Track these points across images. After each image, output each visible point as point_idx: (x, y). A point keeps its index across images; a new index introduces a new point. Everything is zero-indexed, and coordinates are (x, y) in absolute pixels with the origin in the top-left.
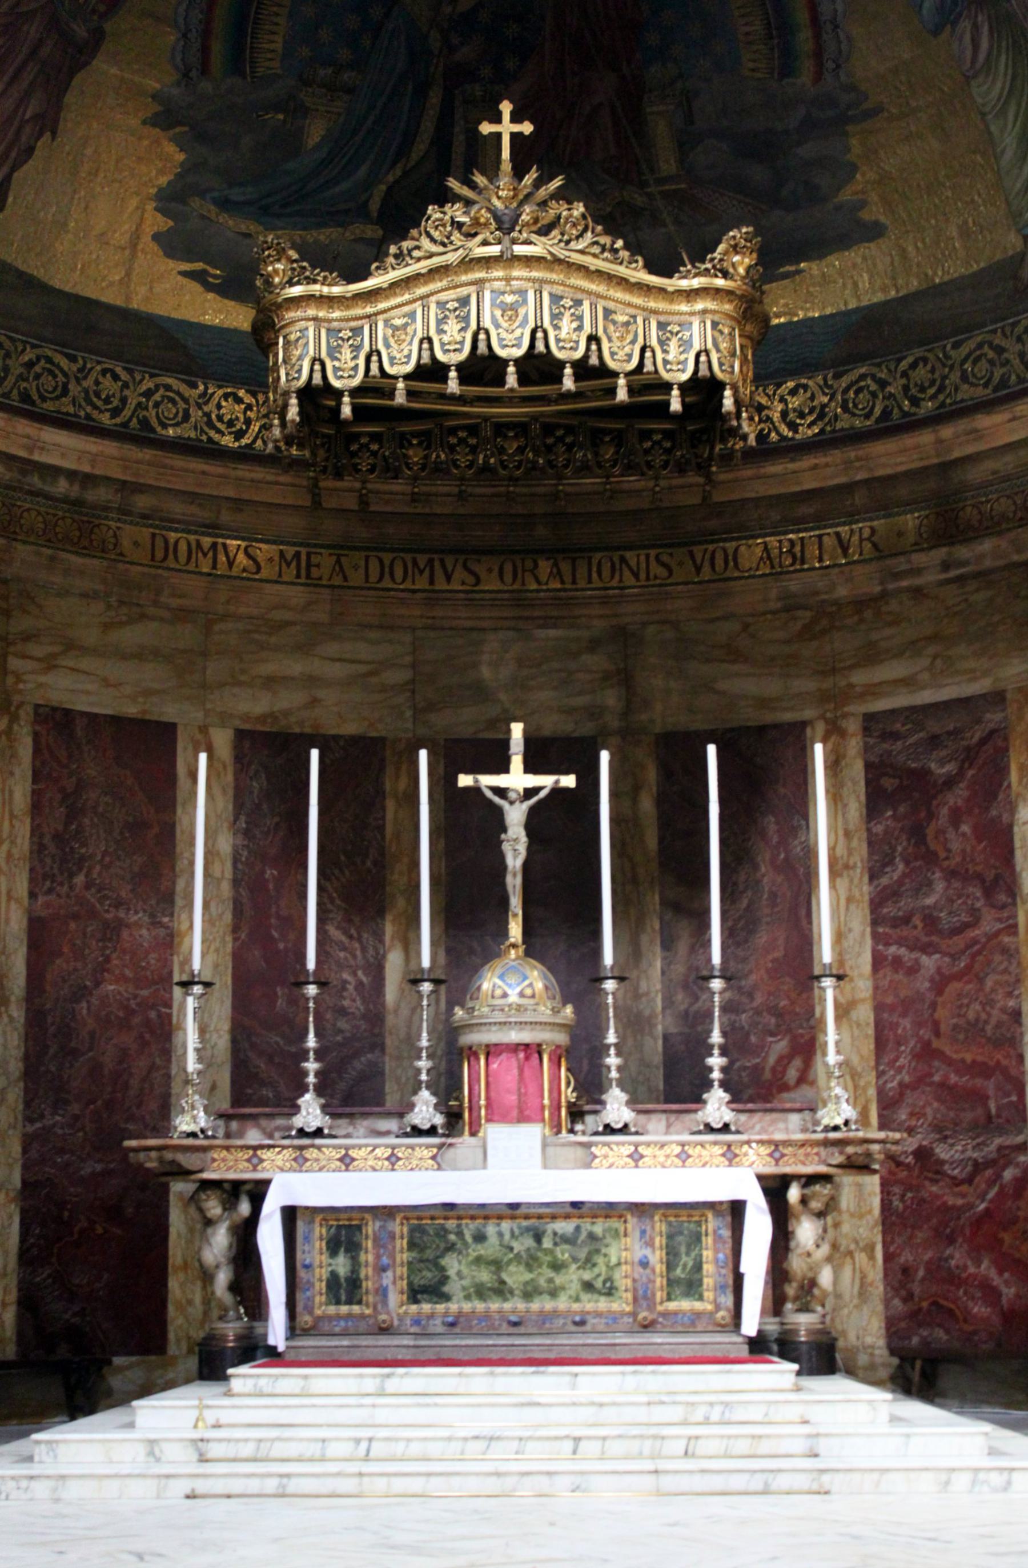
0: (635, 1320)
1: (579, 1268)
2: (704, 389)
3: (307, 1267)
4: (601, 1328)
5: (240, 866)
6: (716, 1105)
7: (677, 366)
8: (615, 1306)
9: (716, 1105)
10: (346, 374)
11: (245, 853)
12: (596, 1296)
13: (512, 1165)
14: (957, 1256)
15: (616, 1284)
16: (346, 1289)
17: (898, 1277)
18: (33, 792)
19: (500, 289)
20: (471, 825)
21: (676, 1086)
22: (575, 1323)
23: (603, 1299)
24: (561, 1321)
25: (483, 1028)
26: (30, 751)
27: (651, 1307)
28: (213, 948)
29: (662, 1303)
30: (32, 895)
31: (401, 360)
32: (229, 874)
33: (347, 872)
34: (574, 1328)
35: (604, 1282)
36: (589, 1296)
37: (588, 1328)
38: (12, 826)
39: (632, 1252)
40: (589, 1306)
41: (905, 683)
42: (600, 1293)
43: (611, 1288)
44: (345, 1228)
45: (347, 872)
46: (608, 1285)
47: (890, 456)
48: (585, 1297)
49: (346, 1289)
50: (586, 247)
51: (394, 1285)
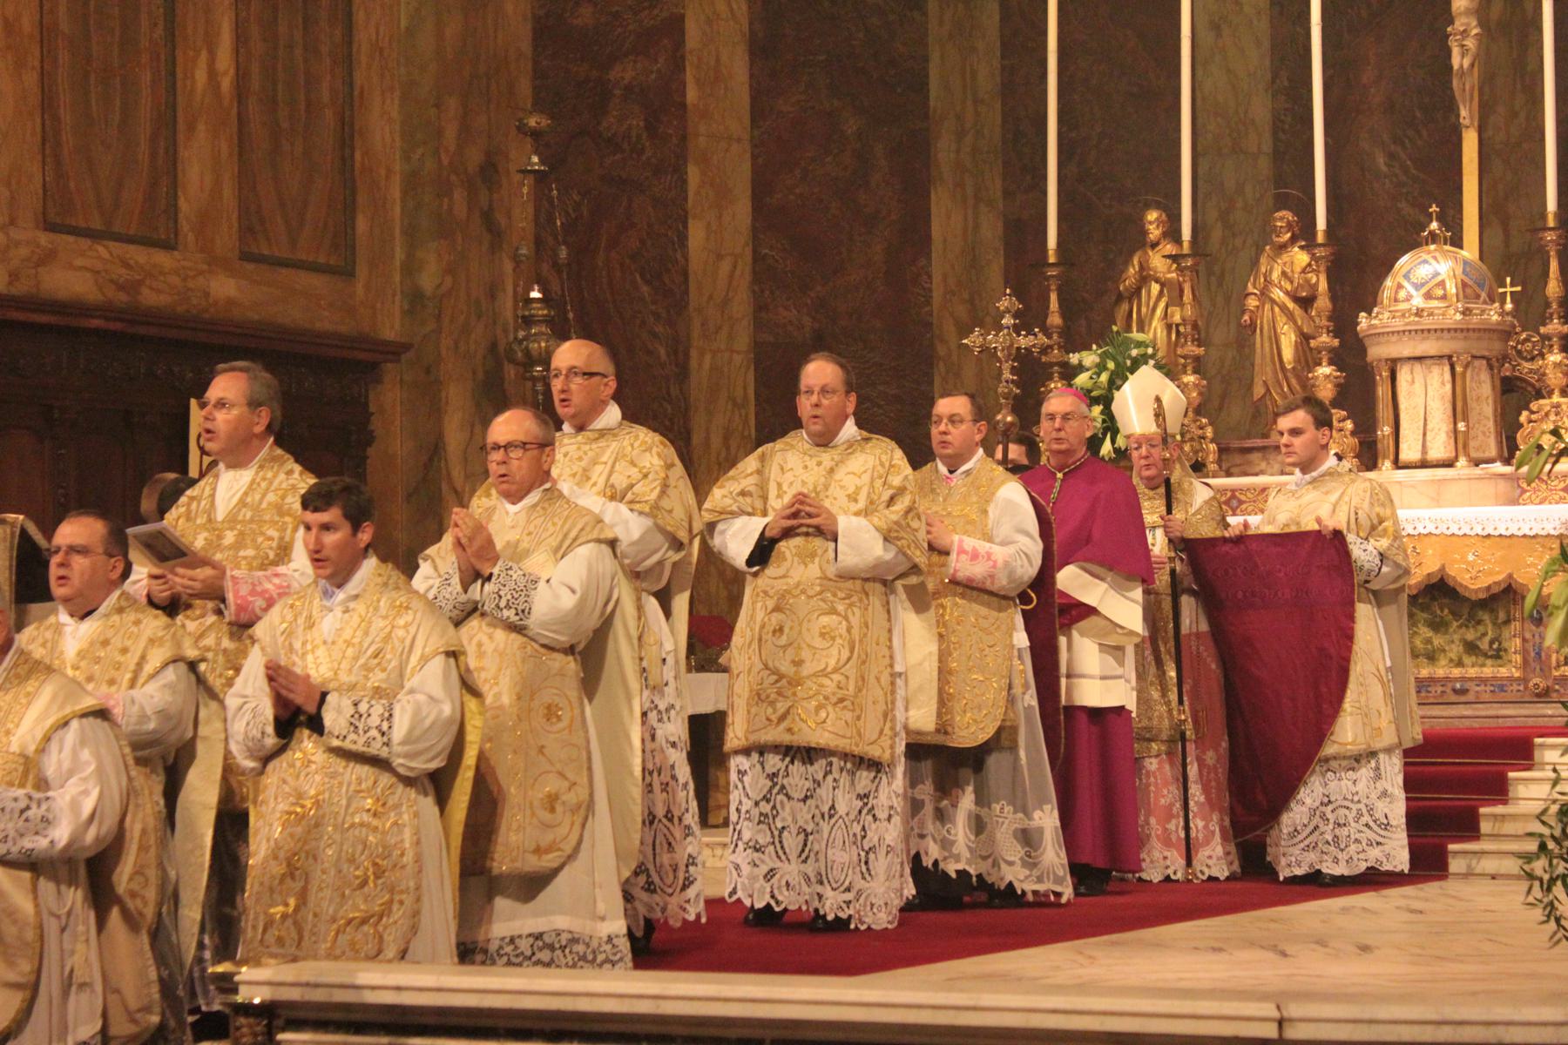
0: (1526, 688)
1: (1460, 627)
3: (137, 623)
4: (1487, 697)
5: (1281, 135)
8: (1503, 672)
11: (1289, 119)
12: (1481, 659)
15: (1505, 645)
18: (1003, 68)
22: (1455, 691)
23: (1489, 662)
24: (1440, 689)
25: (1382, 339)
26: (997, 17)
27: (1545, 671)
28: (1250, 241)
29: (1558, 666)
30: (1007, 194)
32: (1267, 146)
33: (1425, 133)
34: (1454, 698)
35: (1491, 643)
36: (1474, 658)
37: (1471, 697)
38: (977, 114)
40: (1472, 672)
42: (1486, 656)
43: (1499, 650)
45: (1425, 133)
46: (1495, 646)
48: (1467, 660)
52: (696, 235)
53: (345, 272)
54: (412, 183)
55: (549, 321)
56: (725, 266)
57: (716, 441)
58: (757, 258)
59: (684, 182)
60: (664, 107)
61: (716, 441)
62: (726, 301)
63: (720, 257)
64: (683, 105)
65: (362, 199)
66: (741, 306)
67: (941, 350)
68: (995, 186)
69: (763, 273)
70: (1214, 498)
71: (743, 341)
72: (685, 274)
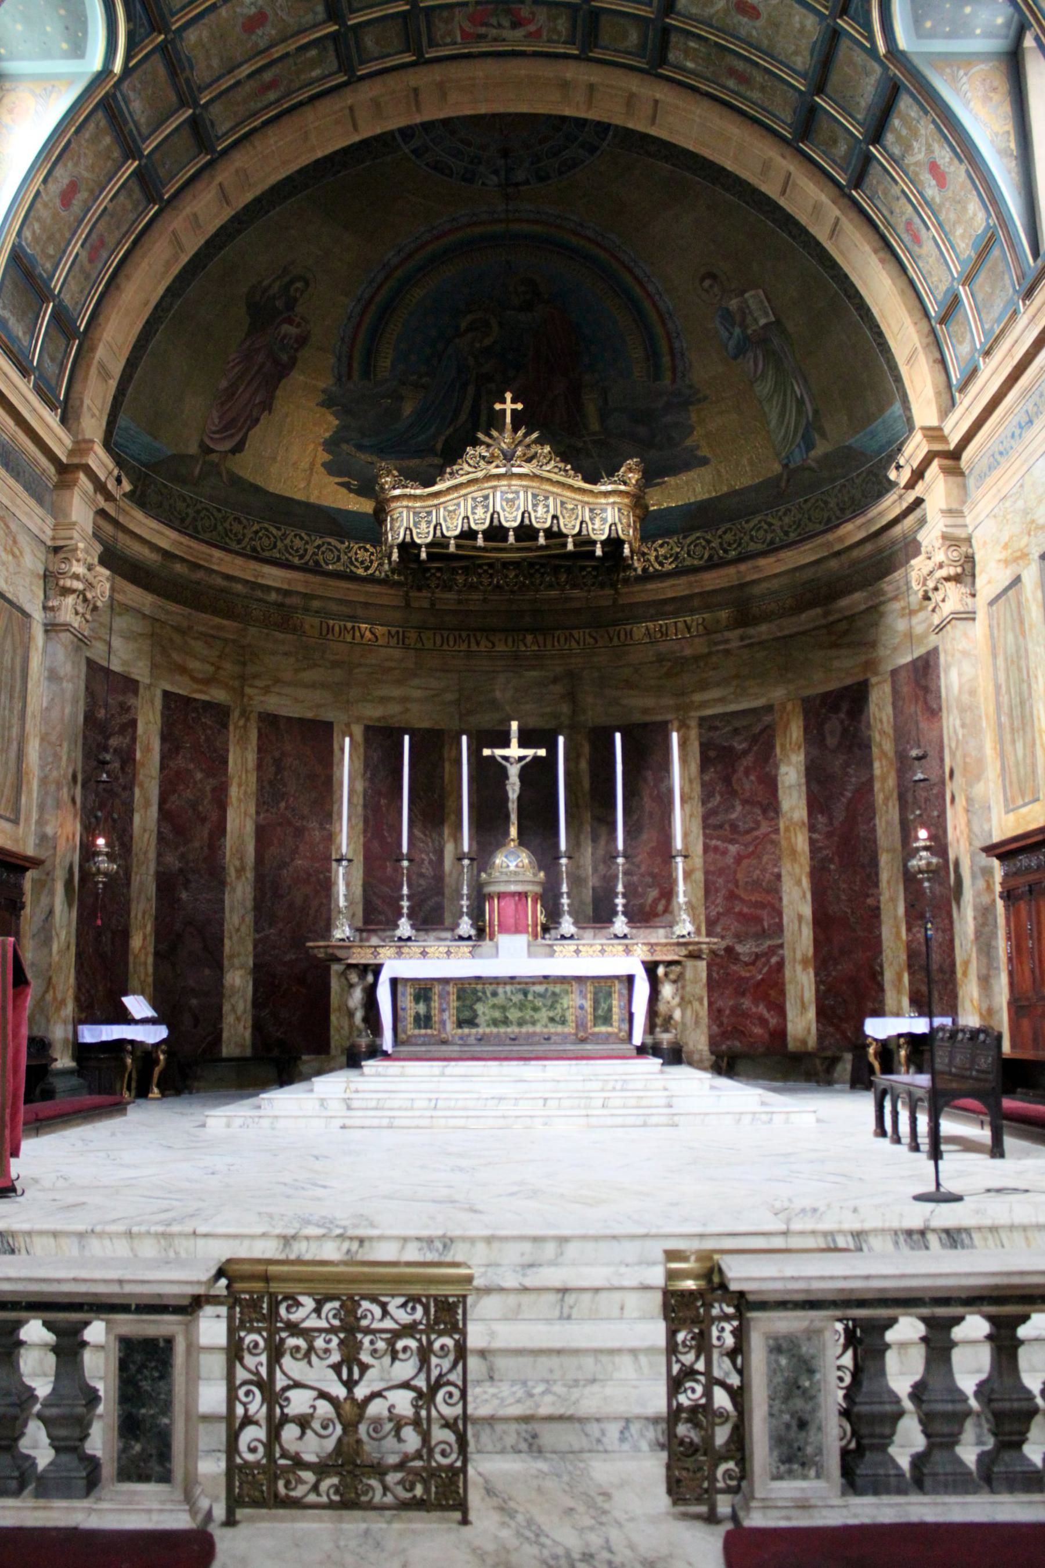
2: (614, 544)
6: (620, 924)
7: (599, 531)
9: (620, 924)
10: (423, 536)
13: (512, 956)
14: (746, 1003)
16: (424, 1021)
17: (715, 1013)
19: (504, 492)
20: (490, 775)
21: (598, 915)
30: (258, 813)
31: (453, 528)
32: (361, 801)
39: (576, 1003)
40: (553, 1030)
41: (717, 701)
44: (423, 989)
47: (713, 580)
49: (424, 1021)
50: (551, 469)
51: (449, 1018)
52: (137, 818)
53: (16, 822)
54: (44, 781)
55: (107, 854)
56: (146, 836)
57: (140, 916)
58: (159, 833)
59: (133, 794)
60: (127, 758)
61: (140, 916)
62: (146, 853)
63: (145, 831)
64: (134, 760)
65: (24, 788)
66: (152, 855)
67: (228, 880)
68: (252, 810)
69: (161, 838)
70: (922, 996)
71: (152, 871)
72: (131, 837)
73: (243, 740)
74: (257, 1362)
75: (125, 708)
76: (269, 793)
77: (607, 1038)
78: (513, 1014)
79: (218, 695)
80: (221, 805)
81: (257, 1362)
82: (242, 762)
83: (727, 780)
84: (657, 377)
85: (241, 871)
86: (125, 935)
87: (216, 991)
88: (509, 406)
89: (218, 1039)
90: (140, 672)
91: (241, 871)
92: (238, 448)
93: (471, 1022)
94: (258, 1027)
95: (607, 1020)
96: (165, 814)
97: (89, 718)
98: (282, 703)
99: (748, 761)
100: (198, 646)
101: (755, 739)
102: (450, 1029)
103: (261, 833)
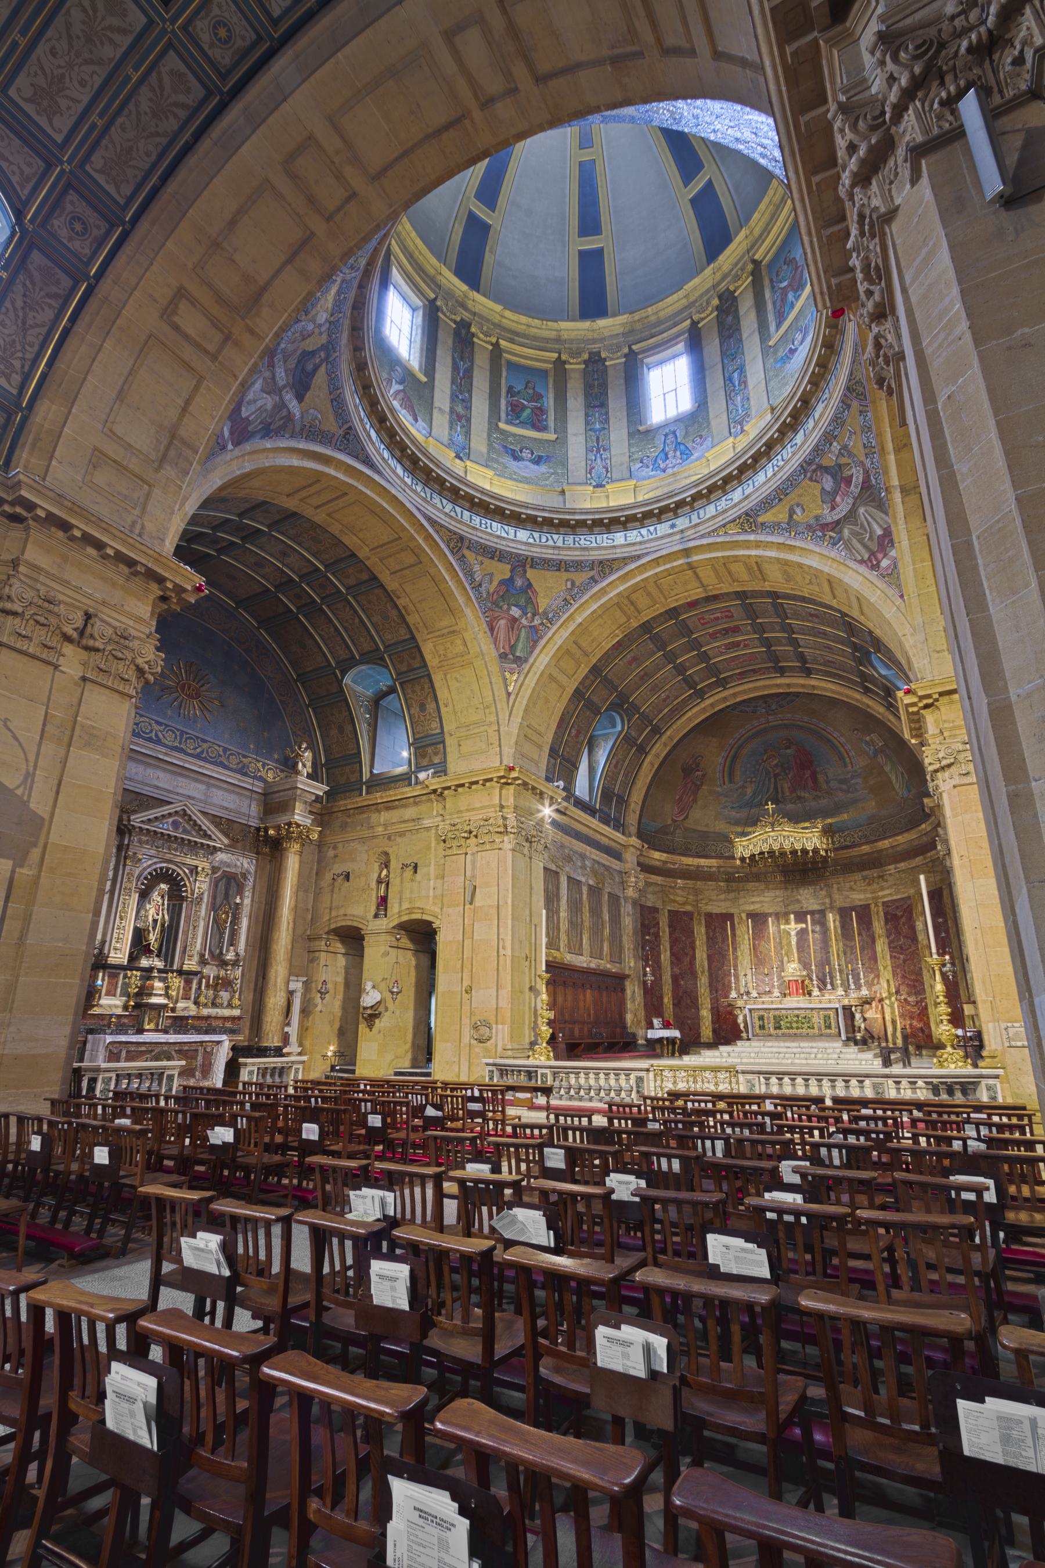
2: (816, 851)
16: (762, 1027)
51: (771, 1026)
69: (672, 963)
73: (700, 923)
74: (659, 1082)
75: (655, 918)
76: (711, 941)
77: (830, 1035)
78: (794, 1025)
79: (689, 908)
80: (694, 949)
81: (659, 1082)
82: (700, 932)
83: (896, 928)
84: (845, 766)
85: (703, 972)
86: (661, 998)
87: (697, 1018)
88: (770, 806)
89: (699, 1036)
90: (659, 905)
91: (703, 972)
92: (686, 817)
93: (779, 1028)
94: (714, 1031)
95: (829, 1027)
96: (672, 954)
97: (643, 925)
98: (715, 908)
99: (903, 920)
100: (680, 892)
101: (905, 911)
102: (772, 1031)
103: (710, 958)
